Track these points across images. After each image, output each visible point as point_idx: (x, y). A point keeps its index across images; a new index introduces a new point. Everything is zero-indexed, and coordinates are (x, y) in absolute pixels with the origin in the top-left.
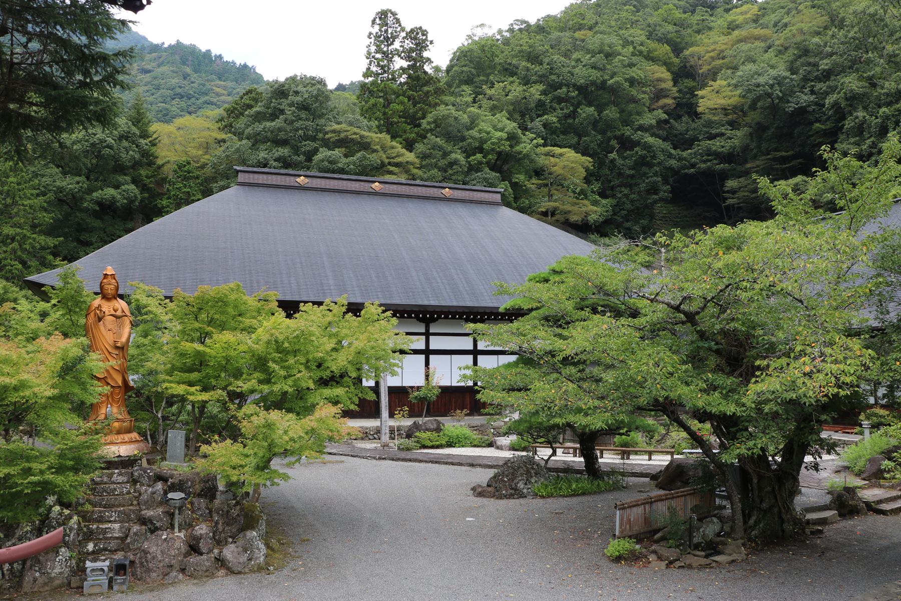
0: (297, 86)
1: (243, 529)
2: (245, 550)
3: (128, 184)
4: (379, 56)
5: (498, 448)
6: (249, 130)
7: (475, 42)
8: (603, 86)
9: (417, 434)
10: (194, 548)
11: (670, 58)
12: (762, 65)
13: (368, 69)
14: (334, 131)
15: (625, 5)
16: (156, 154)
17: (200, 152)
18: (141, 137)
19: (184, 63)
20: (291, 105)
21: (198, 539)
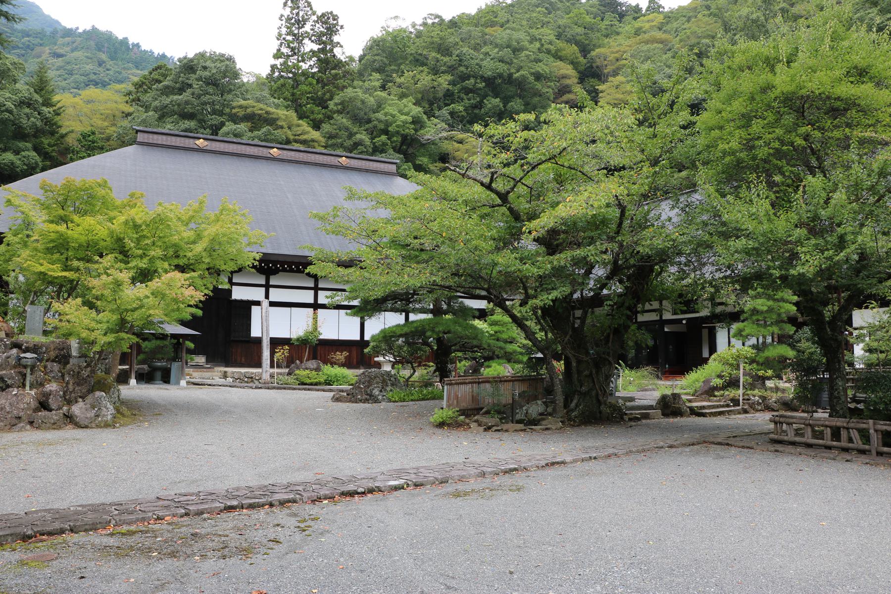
0: (205, 62)
1: (91, 391)
2: (93, 407)
3: (28, 150)
4: (289, 38)
6: (156, 103)
7: (388, 33)
8: (509, 80)
10: (44, 405)
11: (577, 58)
12: (659, 64)
13: (279, 50)
14: (241, 107)
15: (537, 7)
16: (60, 123)
17: (106, 124)
18: (43, 105)
19: (100, 50)
20: (198, 79)
21: (47, 395)
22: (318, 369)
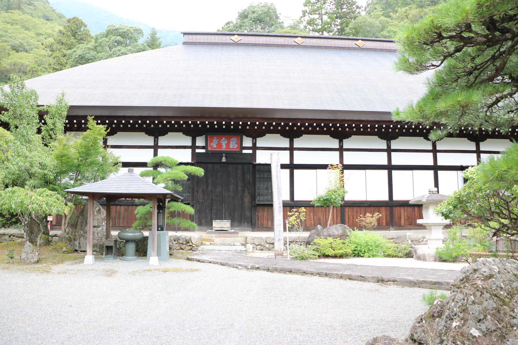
5: (419, 258)
9: (316, 241)
22: (343, 236)
